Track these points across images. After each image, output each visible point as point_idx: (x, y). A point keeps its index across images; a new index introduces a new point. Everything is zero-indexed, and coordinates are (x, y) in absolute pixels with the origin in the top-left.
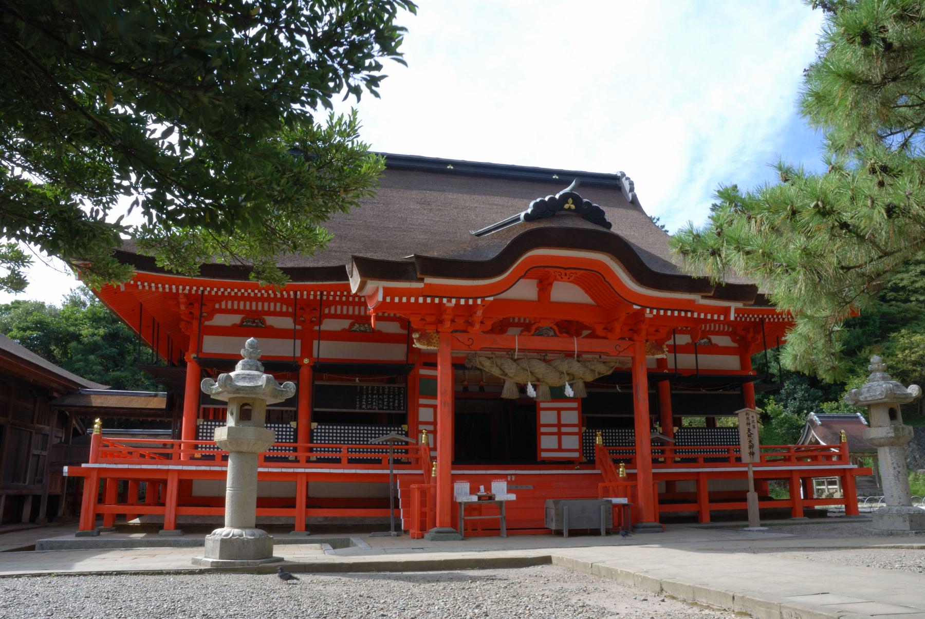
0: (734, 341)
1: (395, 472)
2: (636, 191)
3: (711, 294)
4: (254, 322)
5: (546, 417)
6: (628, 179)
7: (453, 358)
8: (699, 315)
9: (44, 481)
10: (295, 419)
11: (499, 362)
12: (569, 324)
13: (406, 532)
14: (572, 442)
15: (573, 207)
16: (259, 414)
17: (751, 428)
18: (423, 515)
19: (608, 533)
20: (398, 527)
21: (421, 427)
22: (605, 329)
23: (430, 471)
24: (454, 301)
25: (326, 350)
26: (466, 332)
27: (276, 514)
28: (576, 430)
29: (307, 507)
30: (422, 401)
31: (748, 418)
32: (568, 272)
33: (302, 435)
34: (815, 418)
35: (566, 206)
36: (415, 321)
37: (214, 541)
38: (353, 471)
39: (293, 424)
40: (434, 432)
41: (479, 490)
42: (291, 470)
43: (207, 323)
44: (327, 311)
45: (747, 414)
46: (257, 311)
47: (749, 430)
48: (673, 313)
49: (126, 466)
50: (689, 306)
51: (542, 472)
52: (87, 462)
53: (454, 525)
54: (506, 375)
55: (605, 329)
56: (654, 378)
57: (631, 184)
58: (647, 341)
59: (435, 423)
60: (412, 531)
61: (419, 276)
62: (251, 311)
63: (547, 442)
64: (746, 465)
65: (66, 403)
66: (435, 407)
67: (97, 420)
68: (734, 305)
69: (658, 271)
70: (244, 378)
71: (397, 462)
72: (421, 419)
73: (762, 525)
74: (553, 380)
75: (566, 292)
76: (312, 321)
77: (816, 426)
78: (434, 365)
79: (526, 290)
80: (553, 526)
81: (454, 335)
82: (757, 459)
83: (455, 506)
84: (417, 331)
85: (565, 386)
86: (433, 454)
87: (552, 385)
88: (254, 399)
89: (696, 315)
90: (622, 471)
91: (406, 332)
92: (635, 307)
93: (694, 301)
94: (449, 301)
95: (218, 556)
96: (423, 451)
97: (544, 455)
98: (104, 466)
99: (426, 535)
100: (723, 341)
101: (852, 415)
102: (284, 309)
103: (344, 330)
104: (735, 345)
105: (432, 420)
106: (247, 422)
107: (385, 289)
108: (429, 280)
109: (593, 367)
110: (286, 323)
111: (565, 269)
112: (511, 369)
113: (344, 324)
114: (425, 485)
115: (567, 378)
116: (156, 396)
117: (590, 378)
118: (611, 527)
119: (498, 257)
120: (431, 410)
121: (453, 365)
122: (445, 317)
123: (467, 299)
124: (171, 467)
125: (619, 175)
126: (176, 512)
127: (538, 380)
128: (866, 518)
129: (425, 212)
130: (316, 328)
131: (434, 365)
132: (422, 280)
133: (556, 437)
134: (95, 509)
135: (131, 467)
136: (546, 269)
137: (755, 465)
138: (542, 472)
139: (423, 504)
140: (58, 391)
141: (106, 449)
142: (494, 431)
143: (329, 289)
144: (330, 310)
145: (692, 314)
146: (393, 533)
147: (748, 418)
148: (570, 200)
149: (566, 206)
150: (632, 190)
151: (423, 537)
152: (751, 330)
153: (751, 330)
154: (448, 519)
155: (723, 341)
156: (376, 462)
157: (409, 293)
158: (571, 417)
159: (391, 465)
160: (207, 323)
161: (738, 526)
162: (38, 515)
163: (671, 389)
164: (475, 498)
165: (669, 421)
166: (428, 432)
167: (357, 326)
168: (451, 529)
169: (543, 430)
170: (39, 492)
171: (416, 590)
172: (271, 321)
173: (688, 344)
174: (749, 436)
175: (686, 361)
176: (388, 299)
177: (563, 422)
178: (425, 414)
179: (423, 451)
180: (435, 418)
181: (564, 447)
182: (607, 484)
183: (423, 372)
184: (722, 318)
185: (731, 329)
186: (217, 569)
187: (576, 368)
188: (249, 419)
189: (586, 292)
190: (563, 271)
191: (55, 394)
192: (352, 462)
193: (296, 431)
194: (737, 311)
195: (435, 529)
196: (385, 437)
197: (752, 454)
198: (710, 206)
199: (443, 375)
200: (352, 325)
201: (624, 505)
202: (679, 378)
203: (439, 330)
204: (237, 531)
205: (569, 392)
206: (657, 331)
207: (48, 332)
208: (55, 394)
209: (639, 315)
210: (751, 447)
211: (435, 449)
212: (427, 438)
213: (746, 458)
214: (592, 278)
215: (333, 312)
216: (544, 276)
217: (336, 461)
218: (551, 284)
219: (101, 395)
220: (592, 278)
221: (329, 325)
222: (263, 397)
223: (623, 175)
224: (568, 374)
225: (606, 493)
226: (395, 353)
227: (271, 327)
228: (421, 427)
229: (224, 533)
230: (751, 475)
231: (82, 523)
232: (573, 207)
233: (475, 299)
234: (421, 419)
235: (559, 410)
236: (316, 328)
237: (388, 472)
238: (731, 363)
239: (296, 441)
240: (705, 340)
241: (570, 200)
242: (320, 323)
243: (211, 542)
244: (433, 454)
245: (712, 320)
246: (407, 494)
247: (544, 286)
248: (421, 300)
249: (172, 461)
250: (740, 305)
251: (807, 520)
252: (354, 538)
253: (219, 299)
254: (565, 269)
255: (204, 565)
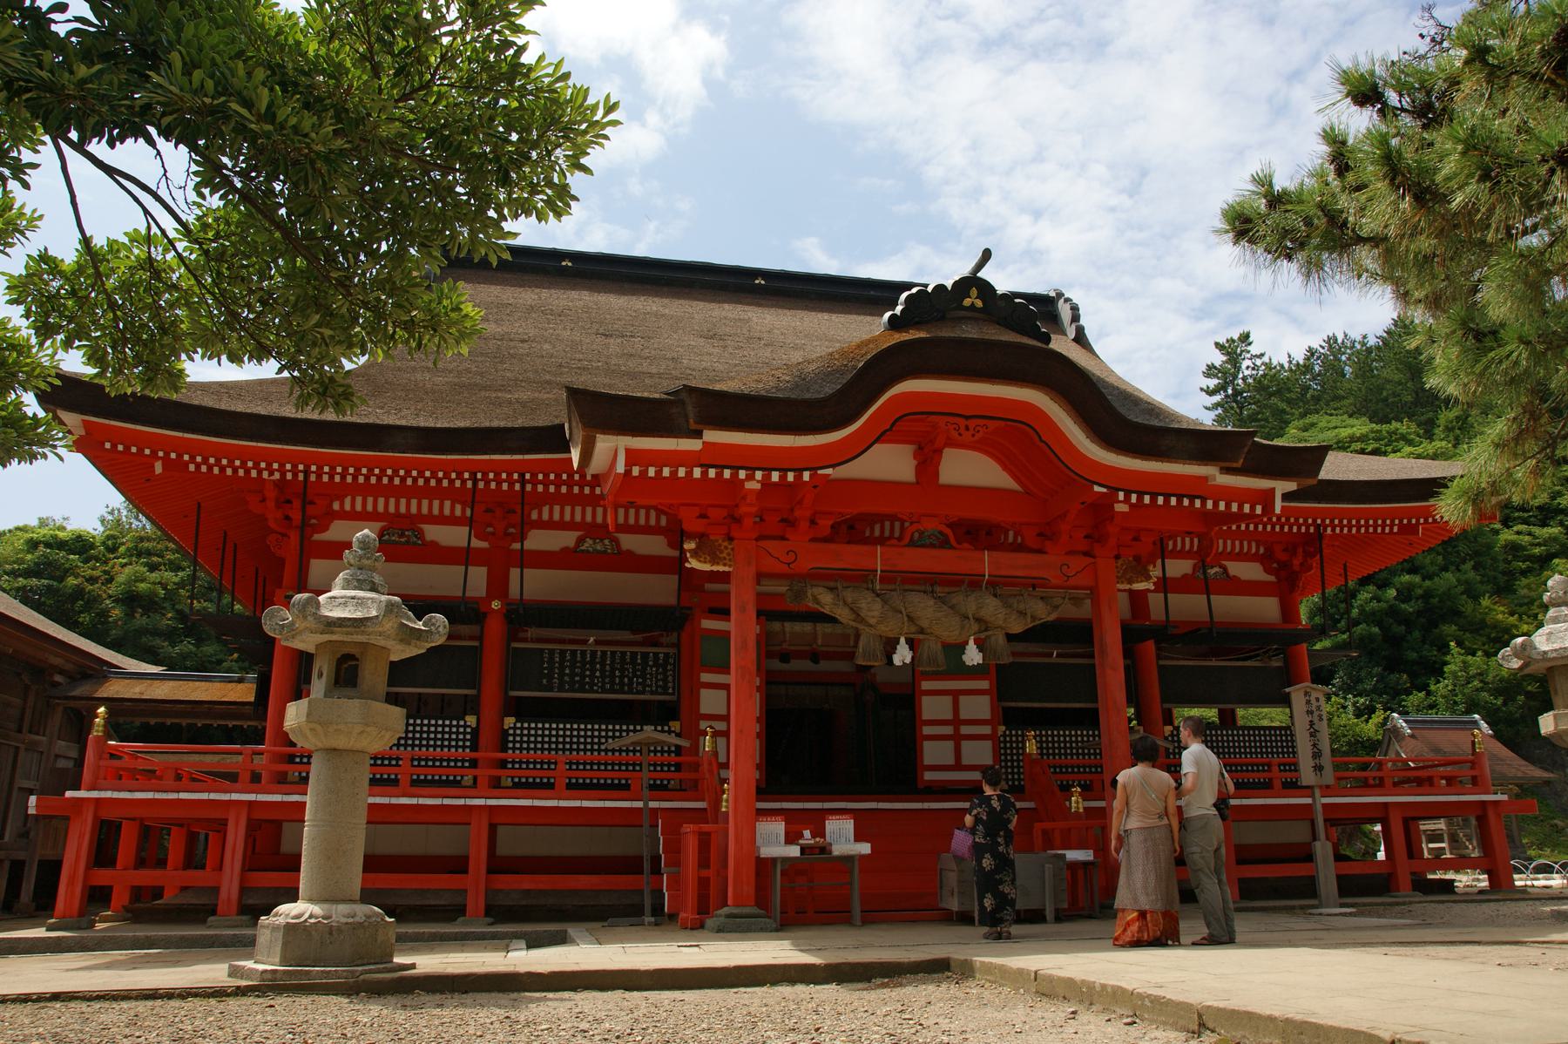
0: (1267, 571)
1: (653, 804)
2: (1082, 322)
3: (1239, 464)
4: (402, 535)
5: (933, 708)
6: (1067, 300)
7: (760, 597)
8: (1216, 505)
9: (32, 834)
10: (476, 711)
11: (849, 595)
12: (975, 526)
13: (672, 917)
14: (979, 753)
15: (979, 303)
16: (374, 675)
17: (1316, 720)
18: (703, 883)
19: (1059, 919)
20: (657, 910)
21: (703, 725)
22: (1040, 535)
23: (718, 802)
24: (759, 475)
25: (535, 584)
26: (783, 538)
27: (420, 886)
28: (987, 730)
29: (489, 871)
30: (706, 677)
31: (1308, 702)
32: (972, 423)
33: (486, 738)
34: (1401, 723)
35: (967, 302)
36: (691, 523)
37: (275, 928)
38: (577, 803)
39: (471, 720)
40: (726, 734)
41: (802, 836)
42: (461, 802)
43: (316, 537)
44: (534, 516)
45: (1306, 694)
46: (408, 515)
47: (1312, 723)
48: (1167, 501)
49: (150, 795)
50: (1198, 488)
51: (926, 805)
52: (77, 787)
53: (762, 900)
54: (862, 620)
55: (1040, 535)
56: (1132, 635)
57: (1075, 309)
58: (1117, 557)
59: (725, 718)
60: (682, 915)
61: (693, 426)
62: (397, 514)
63: (935, 753)
64: (1308, 790)
65: (77, 692)
66: (726, 687)
67: (102, 710)
68: (1282, 487)
69: (1139, 420)
70: (345, 602)
71: (658, 789)
72: (704, 710)
73: (1342, 905)
74: (949, 629)
75: (967, 468)
76: (507, 534)
77: (1404, 737)
78: (723, 613)
79: (890, 463)
80: (954, 905)
81: (760, 543)
82: (1329, 777)
83: (765, 866)
84: (691, 537)
85: (967, 643)
86: (723, 774)
87: (939, 641)
88: (364, 645)
89: (1210, 505)
90: (1076, 803)
91: (676, 553)
92: (1097, 488)
93: (1205, 479)
94: (750, 477)
95: (277, 960)
96: (706, 766)
97: (929, 776)
98: (108, 794)
99: (709, 922)
100: (1249, 571)
101: (1465, 718)
102: (458, 512)
103: (565, 550)
104: (1272, 578)
105: (724, 712)
106: (348, 691)
107: (629, 452)
108: (713, 436)
109: (1022, 607)
110: (455, 536)
111: (967, 418)
112: (871, 608)
113: (568, 539)
114: (706, 827)
115: (975, 627)
116: (240, 680)
117: (1017, 628)
118: (1066, 906)
119: (841, 393)
120: (723, 693)
121: (760, 613)
122: (743, 509)
123: (784, 471)
124: (235, 797)
125: (1053, 294)
126: (242, 882)
127: (922, 631)
128: (1524, 894)
129: (716, 351)
130: (516, 546)
131: (723, 613)
132: (698, 434)
133: (963, 715)
134: (86, 879)
135: (159, 796)
136: (932, 418)
137: (1327, 790)
138: (926, 805)
139: (704, 862)
140: (62, 672)
141: (116, 763)
142: (835, 735)
143: (534, 467)
144: (540, 514)
145: (1203, 504)
146: (648, 919)
147: (1308, 702)
148: (974, 292)
149: (967, 302)
150: (1076, 318)
151: (701, 926)
152: (1300, 550)
153: (1300, 550)
154: (749, 889)
155: (1249, 571)
156: (620, 789)
157: (675, 458)
158: (978, 707)
159: (646, 792)
160: (316, 537)
161: (1293, 908)
162: (18, 896)
163: (1159, 657)
164: (794, 851)
165: (1158, 715)
166: (716, 734)
167: (589, 541)
168: (755, 910)
169: (927, 730)
170: (21, 855)
171: (140, 1009)
172: (433, 533)
173: (1185, 576)
174: (1312, 735)
175: (1188, 606)
176: (636, 471)
177: (950, 744)
178: (710, 702)
179: (706, 766)
180: (730, 706)
181: (965, 761)
182: (1048, 825)
183: (707, 624)
184: (1259, 510)
185: (1262, 550)
186: (269, 987)
187: (991, 607)
188: (355, 685)
189: (1005, 468)
190: (962, 422)
191: (58, 678)
192: (575, 788)
193: (476, 732)
194: (1287, 497)
195: (725, 910)
196: (633, 737)
197: (1318, 768)
198: (1204, 368)
199: (740, 629)
200: (580, 540)
201: (1085, 864)
202: (1168, 635)
203: (733, 534)
204: (317, 909)
205: (973, 656)
206: (1135, 539)
207: (50, 563)
208: (58, 678)
209: (1103, 507)
210: (1317, 755)
211: (726, 766)
212: (714, 743)
213: (1307, 776)
214: (1013, 437)
215: (545, 516)
216: (926, 432)
217: (546, 787)
218: (939, 452)
219: (138, 678)
220: (1013, 437)
221: (538, 541)
222: (382, 643)
223: (1060, 295)
224: (978, 620)
225: (1049, 844)
226: (659, 590)
227: (434, 544)
228: (703, 725)
229: (294, 913)
230: (1319, 808)
231: (60, 904)
232: (979, 303)
233: (799, 471)
234: (704, 710)
235: (956, 694)
236: (516, 546)
237: (639, 804)
238: (1266, 608)
239: (474, 748)
240: (1216, 569)
241: (974, 292)
242: (522, 538)
243: (268, 932)
244: (723, 774)
245: (1240, 516)
246: (675, 849)
247: (927, 462)
248: (697, 473)
249: (238, 786)
250: (1291, 486)
251: (1419, 897)
252: (572, 930)
253: (342, 491)
254: (967, 418)
255: (248, 978)
